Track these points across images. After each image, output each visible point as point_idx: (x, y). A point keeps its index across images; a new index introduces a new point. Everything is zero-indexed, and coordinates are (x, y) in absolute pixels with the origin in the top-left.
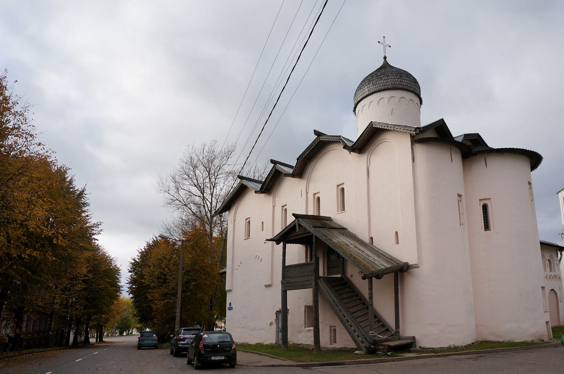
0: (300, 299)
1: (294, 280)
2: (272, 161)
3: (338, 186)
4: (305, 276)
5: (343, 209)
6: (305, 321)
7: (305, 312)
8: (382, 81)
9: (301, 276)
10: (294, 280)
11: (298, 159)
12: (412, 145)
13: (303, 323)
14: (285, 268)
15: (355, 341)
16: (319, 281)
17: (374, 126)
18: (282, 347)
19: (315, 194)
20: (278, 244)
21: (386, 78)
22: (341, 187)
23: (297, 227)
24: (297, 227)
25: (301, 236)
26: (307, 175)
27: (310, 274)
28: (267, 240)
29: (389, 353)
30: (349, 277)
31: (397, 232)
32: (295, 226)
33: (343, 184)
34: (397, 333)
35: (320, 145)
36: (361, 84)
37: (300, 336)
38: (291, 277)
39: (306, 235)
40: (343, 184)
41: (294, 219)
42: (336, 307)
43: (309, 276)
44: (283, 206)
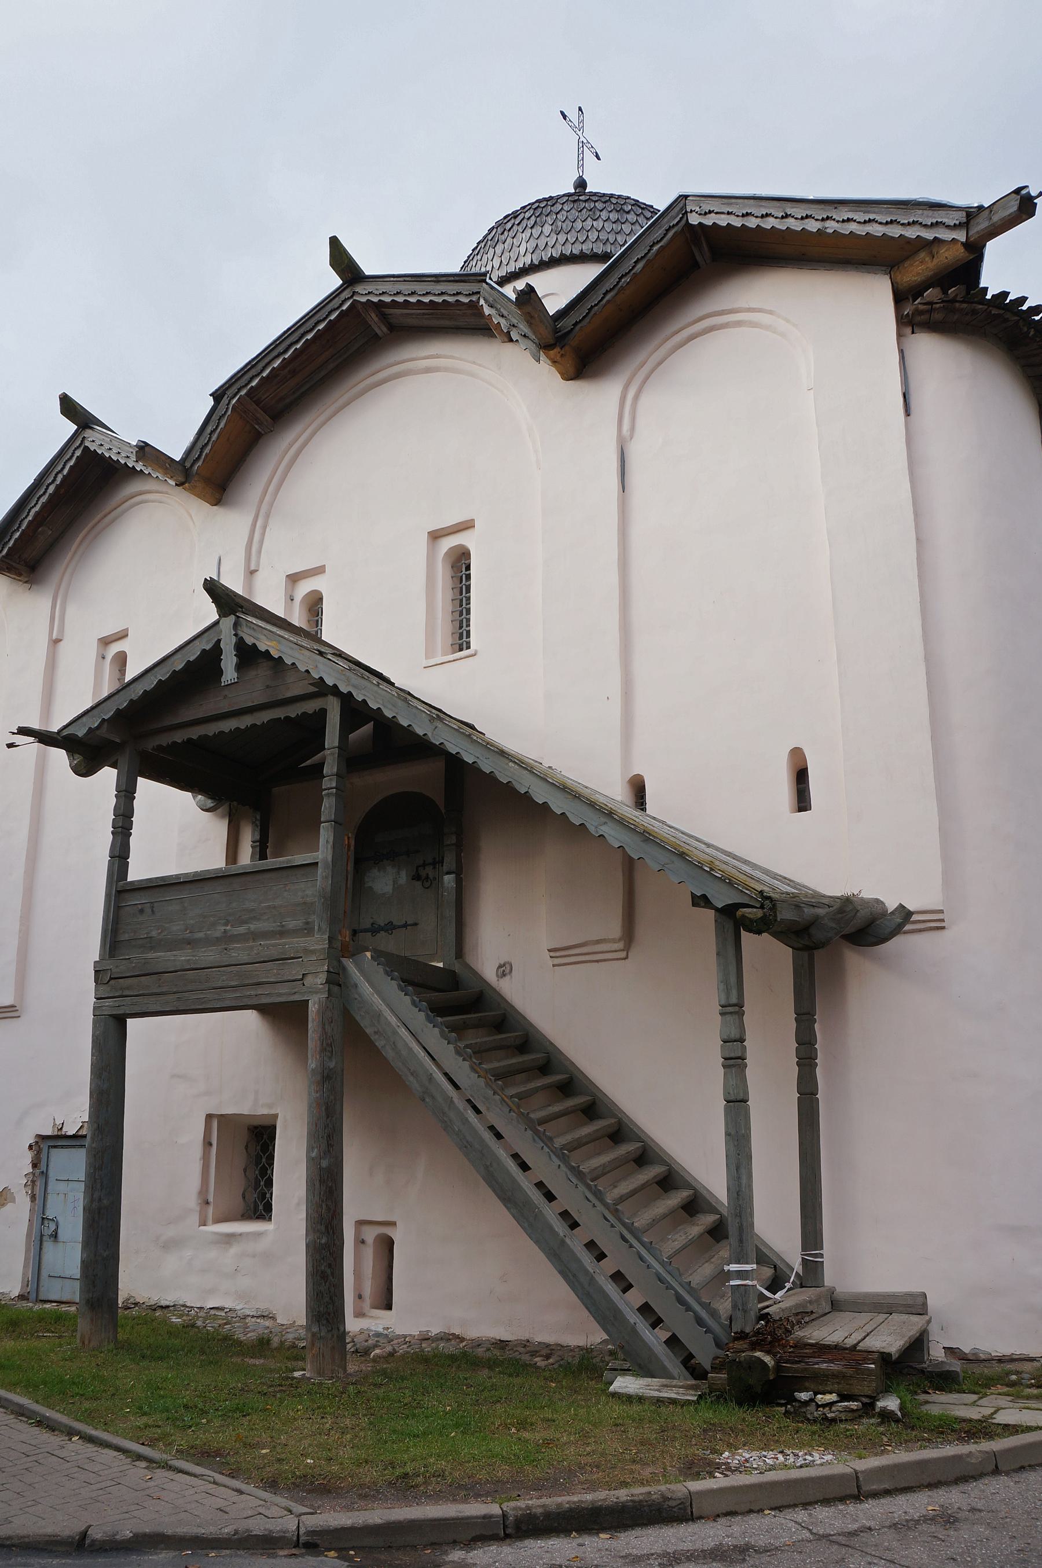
0: (203, 1063)
1: (182, 957)
2: (69, 407)
3: (436, 536)
4: (255, 936)
5: (461, 640)
6: (203, 1191)
7: (207, 1143)
8: (598, 225)
9: (227, 939)
10: (182, 957)
11: (218, 396)
12: (900, 335)
13: (192, 1201)
14: (121, 891)
15: (605, 1314)
16: (349, 964)
17: (694, 220)
18: (83, 1325)
19: (294, 579)
20: (86, 768)
21: (614, 216)
22: (448, 543)
23: (229, 663)
24: (229, 663)
25: (244, 722)
26: (257, 483)
27: (292, 924)
28: (23, 731)
29: (891, 1403)
30: (489, 972)
31: (798, 757)
32: (211, 659)
33: (467, 526)
34: (812, 1270)
35: (355, 333)
36: (499, 224)
37: (172, 1263)
38: (151, 959)
39: (279, 713)
40: (467, 526)
41: (210, 613)
42: (470, 1114)
43: (282, 933)
44: (105, 642)
